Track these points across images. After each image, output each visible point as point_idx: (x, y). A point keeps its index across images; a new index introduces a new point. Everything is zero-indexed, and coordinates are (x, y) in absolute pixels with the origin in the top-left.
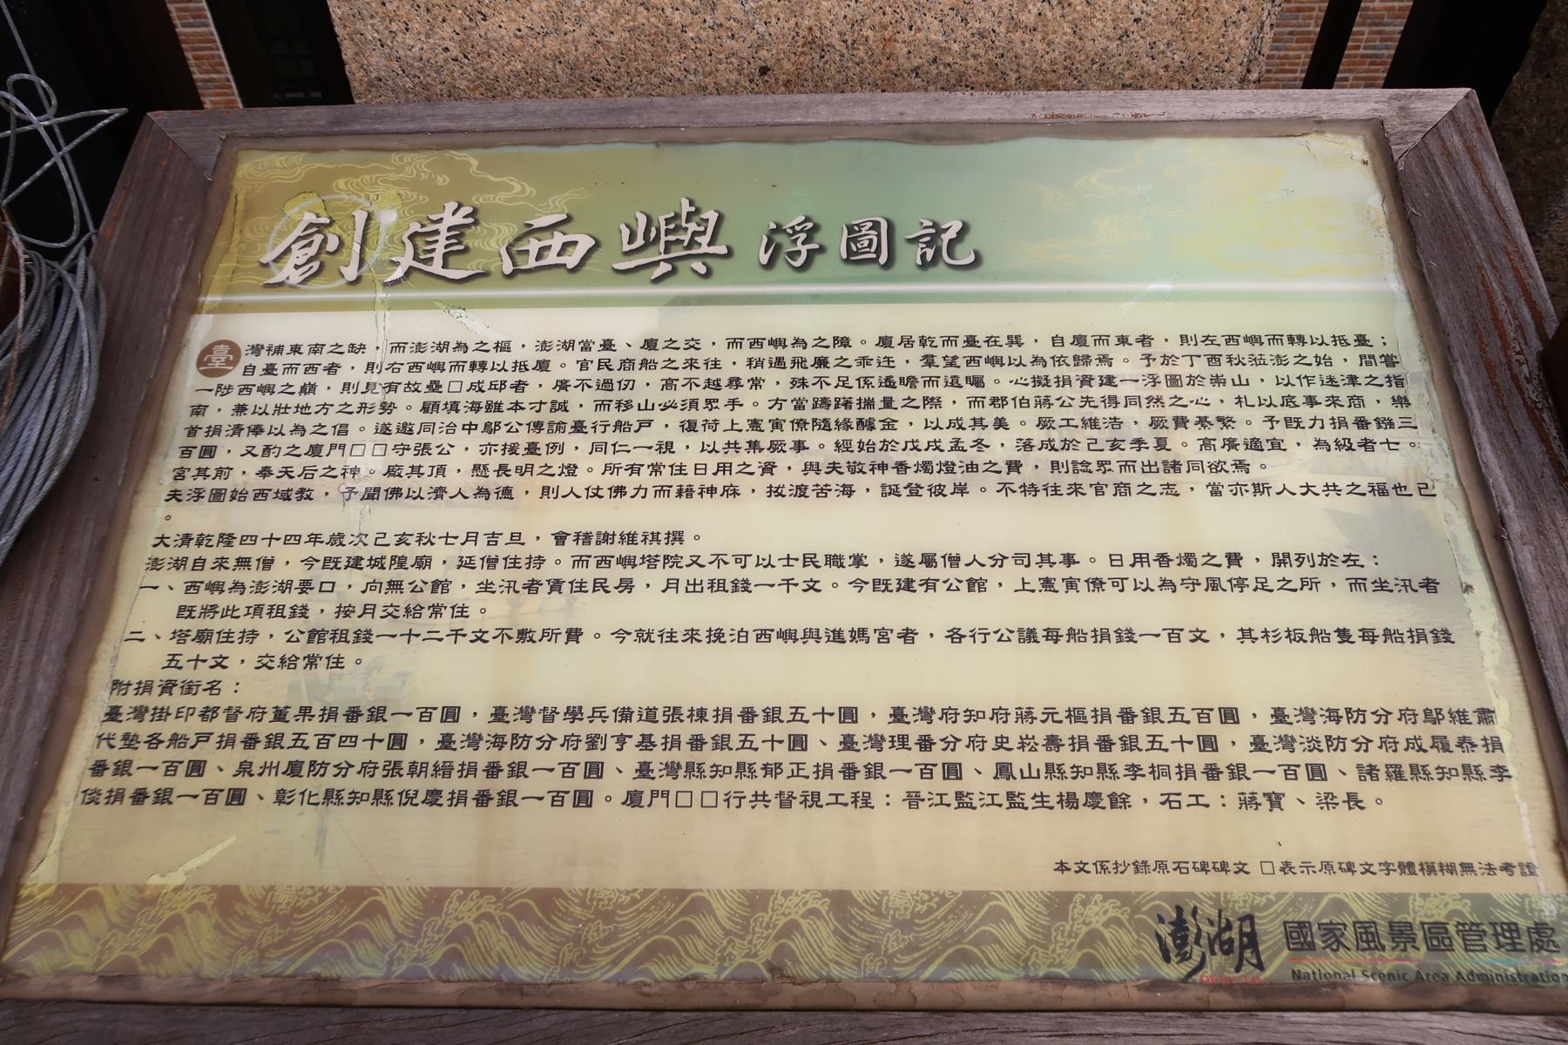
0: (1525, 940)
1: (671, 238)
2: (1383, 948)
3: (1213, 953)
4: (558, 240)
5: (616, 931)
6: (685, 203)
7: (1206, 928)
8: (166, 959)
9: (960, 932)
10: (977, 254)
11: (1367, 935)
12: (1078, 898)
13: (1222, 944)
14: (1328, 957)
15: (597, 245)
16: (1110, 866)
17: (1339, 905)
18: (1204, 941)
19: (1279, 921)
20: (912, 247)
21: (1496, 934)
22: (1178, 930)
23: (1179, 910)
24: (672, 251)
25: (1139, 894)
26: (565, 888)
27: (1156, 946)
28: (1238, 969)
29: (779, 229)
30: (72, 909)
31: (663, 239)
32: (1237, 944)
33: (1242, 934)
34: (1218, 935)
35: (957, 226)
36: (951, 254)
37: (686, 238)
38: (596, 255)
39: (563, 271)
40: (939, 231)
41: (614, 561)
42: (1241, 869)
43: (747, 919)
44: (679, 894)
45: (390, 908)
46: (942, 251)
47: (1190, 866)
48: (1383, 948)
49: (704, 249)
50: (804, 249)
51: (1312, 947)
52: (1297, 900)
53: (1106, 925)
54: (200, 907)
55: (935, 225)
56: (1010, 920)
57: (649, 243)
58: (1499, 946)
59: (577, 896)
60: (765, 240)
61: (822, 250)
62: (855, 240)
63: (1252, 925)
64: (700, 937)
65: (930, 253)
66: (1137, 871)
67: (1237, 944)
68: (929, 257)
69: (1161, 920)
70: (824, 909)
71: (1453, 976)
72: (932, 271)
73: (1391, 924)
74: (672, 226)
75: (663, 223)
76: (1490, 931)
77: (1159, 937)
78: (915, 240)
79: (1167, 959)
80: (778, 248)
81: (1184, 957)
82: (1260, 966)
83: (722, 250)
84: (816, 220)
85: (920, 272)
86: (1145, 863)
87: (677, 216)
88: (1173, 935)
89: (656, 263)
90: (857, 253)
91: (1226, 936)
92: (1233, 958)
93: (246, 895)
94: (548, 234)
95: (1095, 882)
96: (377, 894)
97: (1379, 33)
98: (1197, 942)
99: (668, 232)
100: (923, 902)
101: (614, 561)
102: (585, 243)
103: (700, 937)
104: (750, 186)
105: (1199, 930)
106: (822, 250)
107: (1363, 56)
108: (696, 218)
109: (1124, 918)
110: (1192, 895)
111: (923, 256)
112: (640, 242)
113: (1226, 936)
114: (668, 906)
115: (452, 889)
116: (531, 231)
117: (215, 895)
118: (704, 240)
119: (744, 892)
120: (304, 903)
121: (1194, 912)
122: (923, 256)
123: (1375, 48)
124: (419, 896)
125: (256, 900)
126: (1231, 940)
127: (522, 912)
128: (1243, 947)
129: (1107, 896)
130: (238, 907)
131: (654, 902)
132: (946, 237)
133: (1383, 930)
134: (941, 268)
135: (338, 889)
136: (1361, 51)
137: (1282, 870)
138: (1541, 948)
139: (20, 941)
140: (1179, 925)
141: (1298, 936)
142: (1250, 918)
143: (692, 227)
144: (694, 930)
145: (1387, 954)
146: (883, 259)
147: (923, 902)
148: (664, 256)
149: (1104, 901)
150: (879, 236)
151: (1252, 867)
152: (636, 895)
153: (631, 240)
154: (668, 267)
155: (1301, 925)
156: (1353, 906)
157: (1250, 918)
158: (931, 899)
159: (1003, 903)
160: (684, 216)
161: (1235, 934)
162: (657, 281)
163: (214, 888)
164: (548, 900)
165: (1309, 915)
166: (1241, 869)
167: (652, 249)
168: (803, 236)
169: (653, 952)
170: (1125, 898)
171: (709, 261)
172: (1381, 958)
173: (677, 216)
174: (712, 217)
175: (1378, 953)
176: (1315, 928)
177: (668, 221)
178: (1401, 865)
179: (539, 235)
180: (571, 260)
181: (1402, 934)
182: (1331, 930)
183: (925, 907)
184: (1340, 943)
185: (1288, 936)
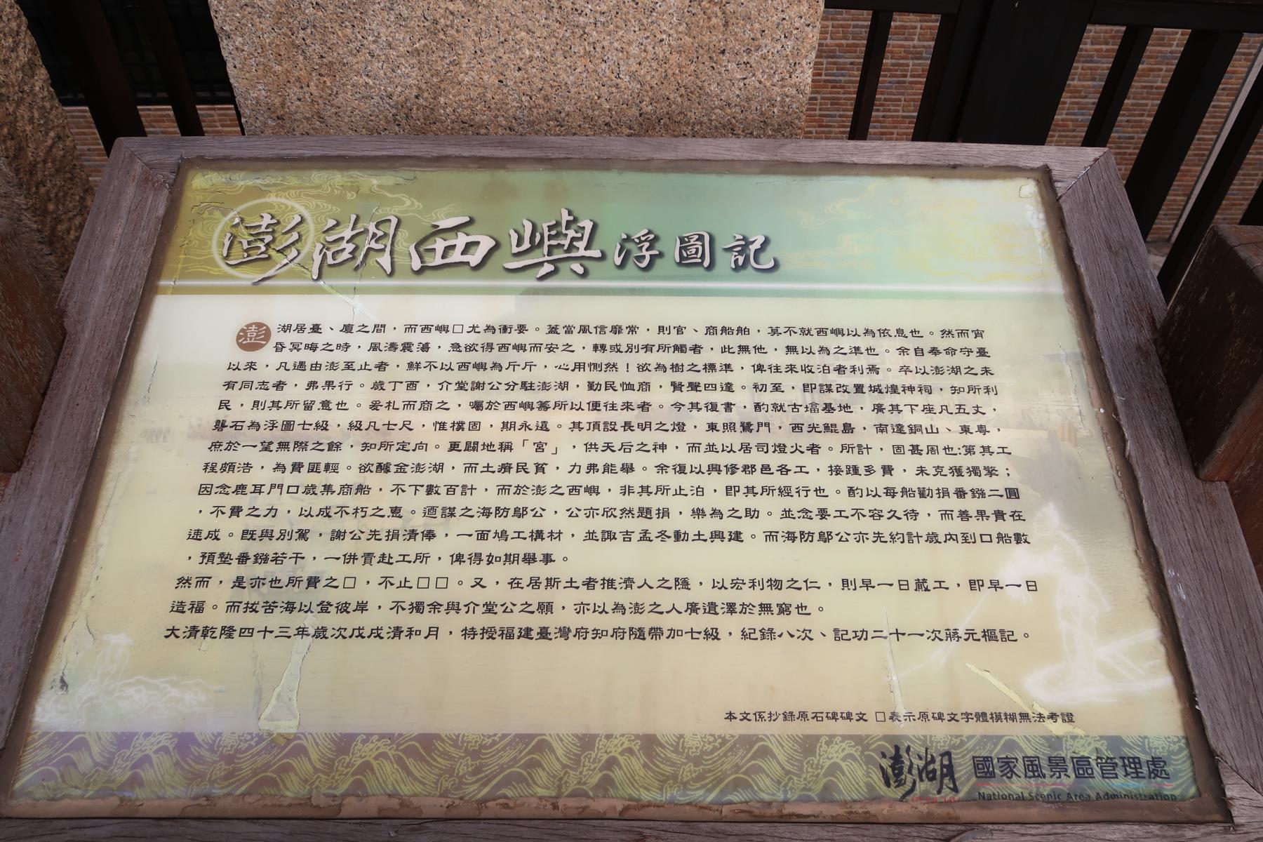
0: (1145, 770)
1: (554, 242)
2: (1044, 776)
3: (921, 780)
4: (461, 240)
5: (235, 770)
6: (565, 213)
7: (916, 762)
8: (137, 790)
9: (737, 765)
10: (775, 260)
11: (1033, 766)
12: (823, 740)
13: (928, 773)
14: (1004, 782)
15: (497, 246)
16: (766, 716)
17: (1011, 745)
18: (915, 772)
19: (969, 756)
20: (728, 255)
21: (1124, 766)
22: (895, 762)
23: (897, 748)
24: (554, 254)
25: (868, 736)
26: (443, 733)
27: (880, 775)
28: (939, 792)
29: (629, 239)
30: (529, 753)
31: (547, 243)
32: (938, 773)
33: (942, 766)
34: (925, 767)
35: (761, 240)
36: (756, 261)
37: (566, 242)
38: (497, 254)
39: (467, 268)
40: (747, 243)
41: (582, 490)
42: (861, 717)
43: (579, 756)
44: (525, 738)
45: (776, 751)
46: (750, 257)
47: (824, 715)
48: (1044, 776)
49: (582, 252)
50: (647, 254)
51: (993, 775)
52: (986, 739)
53: (844, 759)
54: (630, 751)
55: (744, 239)
56: (774, 756)
57: (534, 247)
58: (1127, 774)
59: (451, 739)
60: (619, 247)
61: (661, 255)
62: (686, 248)
63: (950, 760)
64: (544, 769)
65: (741, 259)
66: (785, 719)
67: (938, 773)
68: (740, 263)
69: (884, 756)
70: (636, 748)
71: (1093, 796)
72: (743, 272)
73: (1050, 759)
74: (553, 233)
75: (546, 230)
76: (1120, 763)
77: (882, 768)
78: (730, 250)
79: (888, 784)
80: (628, 253)
81: (900, 783)
82: (955, 790)
83: (597, 254)
84: (657, 233)
85: (734, 273)
86: (791, 713)
87: (558, 224)
88: (893, 767)
89: (541, 264)
90: (687, 258)
91: (931, 767)
92: (936, 784)
93: (200, 740)
94: (453, 234)
95: (841, 727)
96: (300, 738)
97: (834, 63)
98: (910, 772)
99: (550, 237)
100: (710, 743)
101: (582, 490)
102: (486, 244)
103: (544, 769)
104: (620, 203)
105: (912, 764)
106: (661, 255)
107: (825, 81)
108: (574, 226)
109: (857, 755)
110: (907, 738)
111: (736, 261)
112: (526, 245)
113: (931, 767)
114: (520, 746)
115: (356, 735)
116: (438, 232)
117: (176, 740)
118: (581, 245)
119: (576, 736)
120: (244, 746)
121: (908, 749)
122: (736, 261)
123: (833, 75)
124: (795, 740)
125: (208, 744)
126: (934, 771)
127: (410, 752)
128: (943, 776)
129: (845, 738)
130: (194, 749)
131: (510, 743)
132: (753, 248)
133: (1044, 763)
134: (749, 271)
135: (733, 736)
136: (823, 77)
137: (891, 718)
138: (1156, 776)
139: (30, 772)
140: (897, 759)
141: (983, 767)
142: (948, 754)
143: (571, 233)
144: (539, 764)
145: (1047, 780)
146: (706, 263)
147: (1174, 743)
148: (547, 258)
149: (842, 741)
150: (703, 246)
151: (870, 716)
152: (496, 738)
153: (519, 244)
154: (551, 268)
155: (986, 759)
156: (1023, 746)
157: (948, 754)
158: (715, 740)
159: (305, 743)
160: (564, 224)
161: (937, 766)
162: (542, 278)
163: (175, 735)
164: (428, 741)
165: (991, 752)
166: (861, 717)
167: (537, 252)
168: (647, 245)
169: (507, 782)
170: (858, 740)
171: (586, 263)
172: (1043, 783)
173: (558, 224)
174: (588, 225)
175: (1040, 780)
176: (995, 761)
177: (550, 228)
178: (977, 714)
179: (444, 235)
180: (475, 258)
181: (1057, 764)
182: (1007, 763)
183: (1176, 747)
184: (1013, 772)
185: (976, 766)
